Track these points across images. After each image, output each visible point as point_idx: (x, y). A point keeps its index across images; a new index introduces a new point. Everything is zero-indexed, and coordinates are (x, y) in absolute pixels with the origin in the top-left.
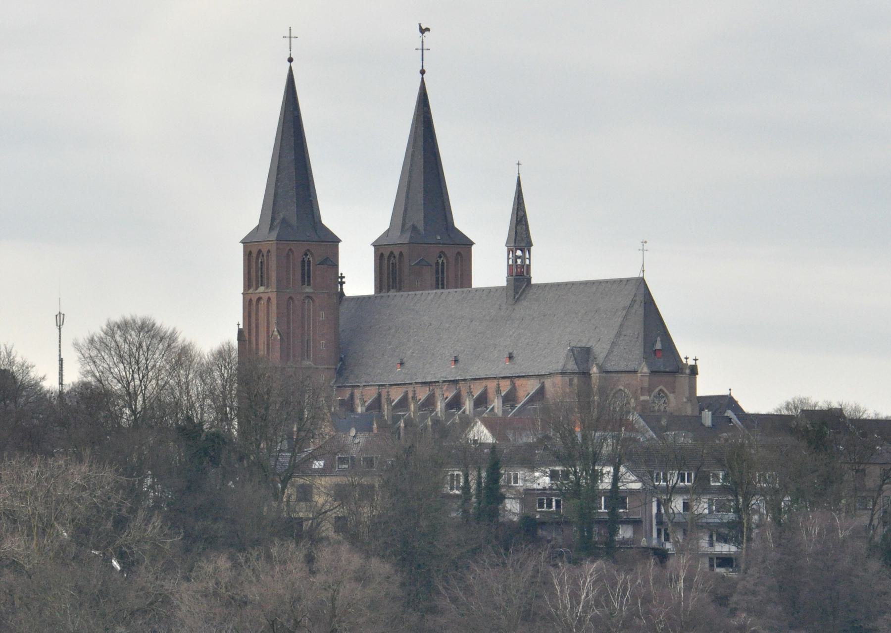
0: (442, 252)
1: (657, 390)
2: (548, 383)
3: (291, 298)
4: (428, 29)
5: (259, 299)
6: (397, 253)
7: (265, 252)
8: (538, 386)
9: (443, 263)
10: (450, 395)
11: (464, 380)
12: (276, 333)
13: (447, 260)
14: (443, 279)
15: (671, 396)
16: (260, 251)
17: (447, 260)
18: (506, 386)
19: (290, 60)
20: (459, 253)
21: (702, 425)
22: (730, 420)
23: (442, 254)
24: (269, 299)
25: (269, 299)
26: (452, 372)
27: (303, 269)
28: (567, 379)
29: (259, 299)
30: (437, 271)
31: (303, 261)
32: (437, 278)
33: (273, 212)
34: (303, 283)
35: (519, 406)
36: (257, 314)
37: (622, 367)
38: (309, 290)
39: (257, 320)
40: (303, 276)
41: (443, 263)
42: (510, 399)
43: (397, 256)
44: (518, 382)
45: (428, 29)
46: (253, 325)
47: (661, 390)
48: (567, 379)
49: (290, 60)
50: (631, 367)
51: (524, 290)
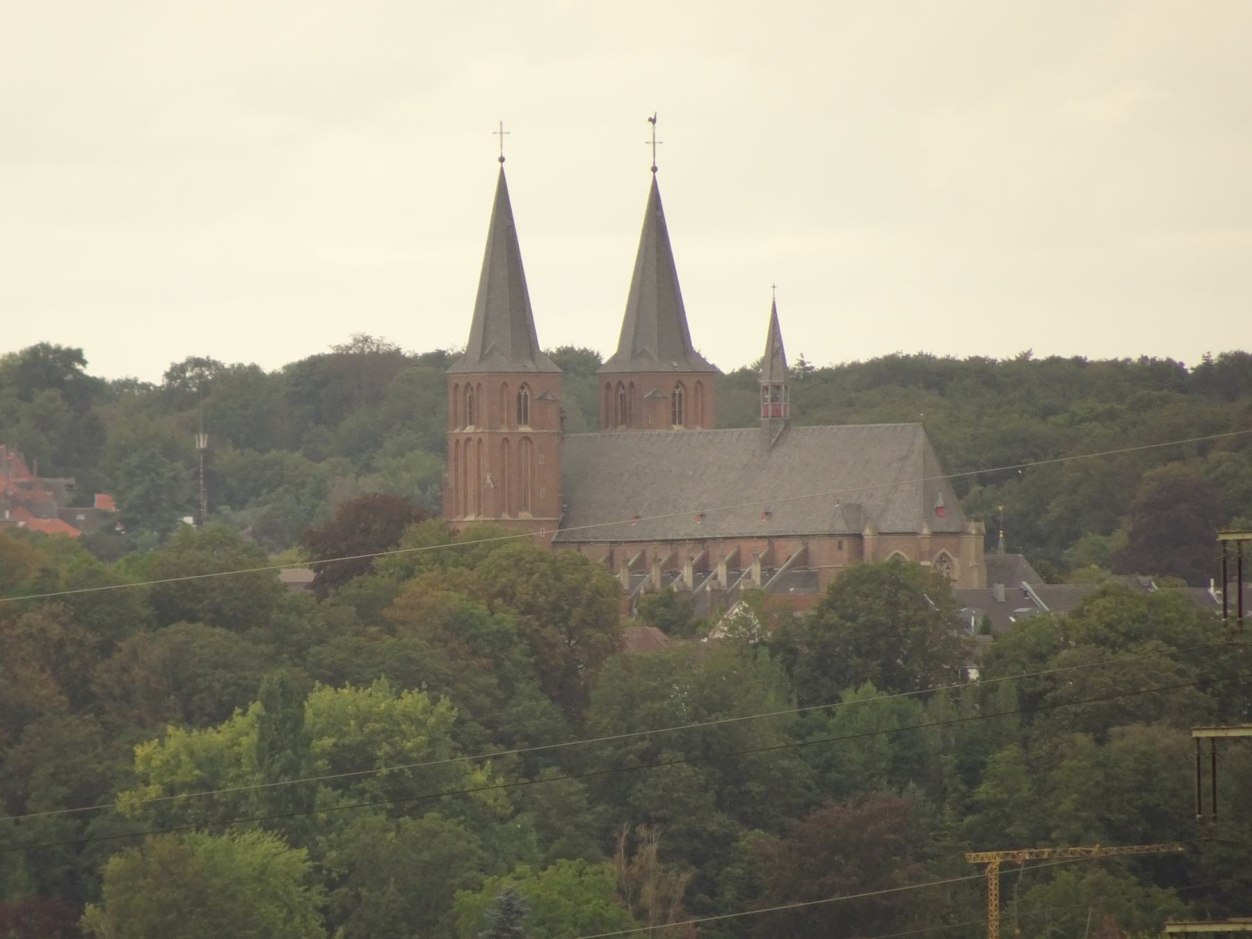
0: (680, 382)
1: (939, 554)
2: (813, 545)
3: (506, 439)
4: (650, 120)
5: (469, 440)
6: (626, 383)
7: (474, 386)
8: (801, 549)
9: (680, 395)
10: (698, 556)
11: (714, 539)
12: (489, 481)
13: (685, 388)
14: (680, 412)
15: (955, 560)
16: (468, 384)
17: (685, 388)
18: (763, 548)
19: (654, 169)
20: (699, 382)
21: (994, 599)
22: (1026, 593)
23: (679, 384)
24: (480, 440)
25: (480, 440)
26: (695, 529)
27: (519, 404)
28: (836, 541)
29: (469, 440)
30: (674, 404)
31: (519, 396)
32: (674, 412)
33: (484, 338)
34: (520, 422)
35: (780, 570)
36: (465, 458)
37: (900, 527)
38: (525, 429)
39: (465, 464)
40: (519, 411)
41: (680, 395)
42: (768, 564)
43: (627, 387)
44: (778, 543)
45: (650, 120)
46: (461, 470)
47: (944, 554)
48: (836, 541)
49: (654, 169)
50: (909, 527)
51: (781, 434)
